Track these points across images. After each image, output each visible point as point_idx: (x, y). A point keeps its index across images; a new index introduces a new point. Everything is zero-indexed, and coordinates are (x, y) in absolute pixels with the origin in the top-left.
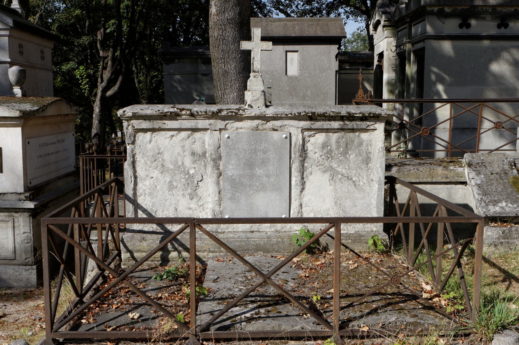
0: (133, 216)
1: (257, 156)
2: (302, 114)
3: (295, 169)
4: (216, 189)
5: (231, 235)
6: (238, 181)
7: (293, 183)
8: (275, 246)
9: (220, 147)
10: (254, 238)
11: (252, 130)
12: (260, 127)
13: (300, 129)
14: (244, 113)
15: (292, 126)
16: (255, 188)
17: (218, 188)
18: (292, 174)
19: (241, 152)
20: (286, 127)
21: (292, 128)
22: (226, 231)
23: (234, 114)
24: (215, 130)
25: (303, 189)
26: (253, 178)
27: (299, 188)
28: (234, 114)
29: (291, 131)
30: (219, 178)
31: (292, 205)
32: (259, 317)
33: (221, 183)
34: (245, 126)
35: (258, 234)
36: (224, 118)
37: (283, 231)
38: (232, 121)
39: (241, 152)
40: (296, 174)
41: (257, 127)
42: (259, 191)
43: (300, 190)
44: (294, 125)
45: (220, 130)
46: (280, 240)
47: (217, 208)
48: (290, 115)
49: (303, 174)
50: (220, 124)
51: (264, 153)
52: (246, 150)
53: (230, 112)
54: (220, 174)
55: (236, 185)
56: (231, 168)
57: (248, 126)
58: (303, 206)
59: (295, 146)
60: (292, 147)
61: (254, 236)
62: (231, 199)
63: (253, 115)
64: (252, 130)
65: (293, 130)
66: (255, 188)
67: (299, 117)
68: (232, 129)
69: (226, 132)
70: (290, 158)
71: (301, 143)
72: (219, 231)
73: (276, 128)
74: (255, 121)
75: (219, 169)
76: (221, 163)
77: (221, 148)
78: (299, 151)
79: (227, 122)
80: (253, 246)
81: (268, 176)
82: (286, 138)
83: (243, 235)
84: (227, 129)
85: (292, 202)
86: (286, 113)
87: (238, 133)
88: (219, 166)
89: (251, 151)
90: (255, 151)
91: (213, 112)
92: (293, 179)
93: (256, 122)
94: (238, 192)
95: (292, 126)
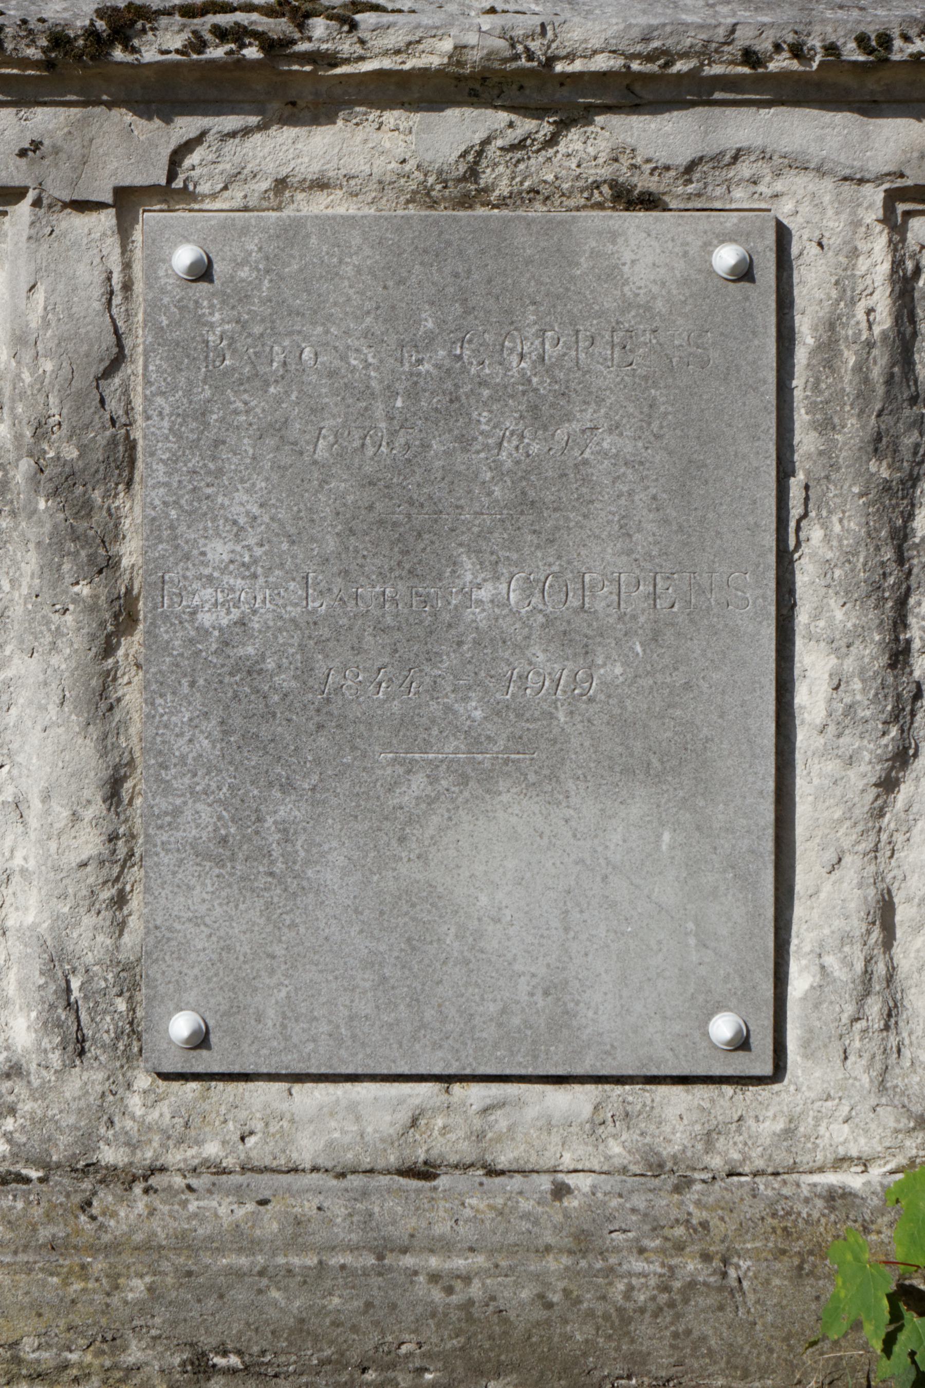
0: (112, 211)
1: (465, 442)
2: (901, 51)
3: (827, 567)
4: (87, 749)
5: (226, 1210)
6: (285, 681)
7: (811, 700)
8: (643, 1328)
9: (117, 360)
10: (445, 1246)
11: (424, 197)
12: (498, 176)
13: (875, 195)
14: (347, 47)
15: (798, 164)
16: (453, 747)
17: (105, 745)
18: (802, 618)
19: (317, 410)
20: (745, 169)
21: (800, 183)
22: (175, 1157)
23: (252, 52)
24: (82, 206)
25: (903, 757)
26: (432, 658)
27: (871, 750)
28: (252, 52)
29: (784, 210)
30: (109, 650)
31: (799, 911)
32: (342, 1175)
33: (131, 693)
34: (358, 164)
35: (479, 1199)
36: (161, 94)
37: (716, 1162)
38: (232, 122)
39: (317, 410)
40: (840, 615)
41: (473, 173)
42: (487, 778)
43: (875, 772)
44: (815, 153)
45: (127, 201)
46: (692, 1266)
47: (89, 940)
48: (781, 63)
49: (900, 621)
50: (126, 145)
51: (539, 416)
52: (367, 392)
53: (222, 34)
54: (123, 616)
55: (272, 718)
56: (227, 564)
57: (385, 166)
58: (903, 914)
59: (828, 349)
60: (801, 356)
61: (442, 1228)
62: (220, 851)
63: (435, 61)
64: (424, 197)
65: (801, 204)
66: (453, 747)
67: (872, 84)
68: (236, 196)
69: (181, 217)
70: (785, 470)
71: (884, 320)
72: (110, 1155)
73: (645, 182)
74: (453, 114)
75: (111, 565)
76: (133, 512)
77: (135, 368)
78: (863, 395)
79: (186, 126)
80: (430, 1333)
81: (574, 638)
82: (744, 273)
83: (338, 1209)
84: (187, 195)
85: (802, 880)
86: (744, 38)
87: (292, 232)
88: (112, 534)
89: (413, 394)
90: (452, 403)
91: (59, 39)
92: (814, 665)
93: (455, 131)
94: (287, 787)
95: (798, 164)
